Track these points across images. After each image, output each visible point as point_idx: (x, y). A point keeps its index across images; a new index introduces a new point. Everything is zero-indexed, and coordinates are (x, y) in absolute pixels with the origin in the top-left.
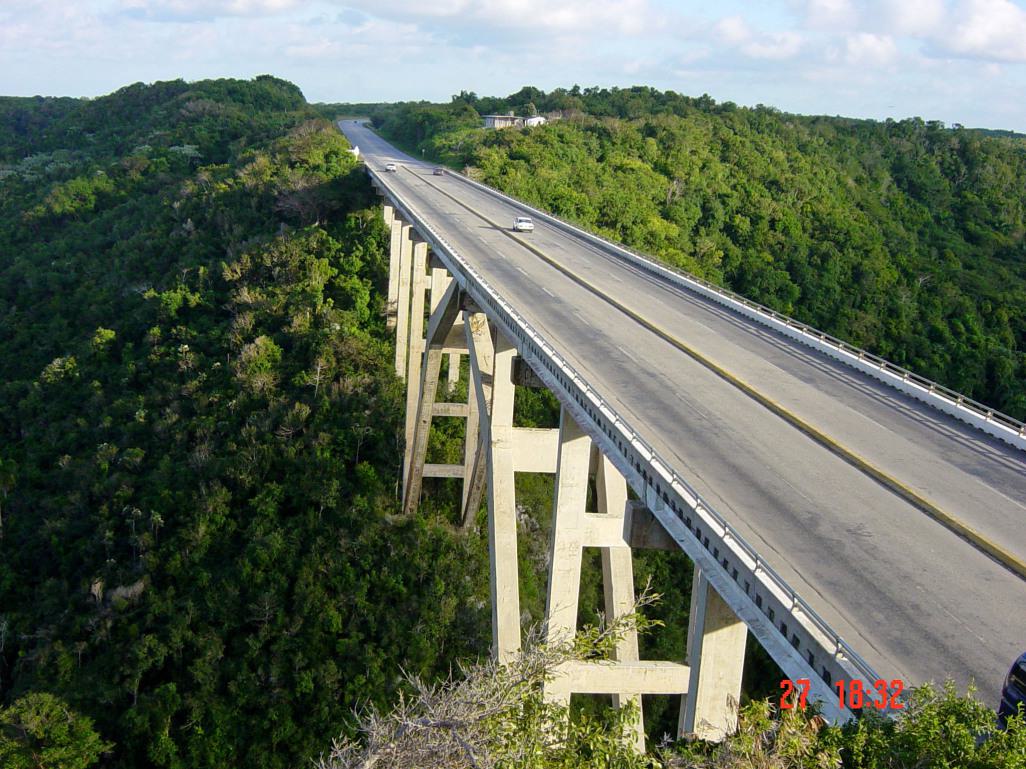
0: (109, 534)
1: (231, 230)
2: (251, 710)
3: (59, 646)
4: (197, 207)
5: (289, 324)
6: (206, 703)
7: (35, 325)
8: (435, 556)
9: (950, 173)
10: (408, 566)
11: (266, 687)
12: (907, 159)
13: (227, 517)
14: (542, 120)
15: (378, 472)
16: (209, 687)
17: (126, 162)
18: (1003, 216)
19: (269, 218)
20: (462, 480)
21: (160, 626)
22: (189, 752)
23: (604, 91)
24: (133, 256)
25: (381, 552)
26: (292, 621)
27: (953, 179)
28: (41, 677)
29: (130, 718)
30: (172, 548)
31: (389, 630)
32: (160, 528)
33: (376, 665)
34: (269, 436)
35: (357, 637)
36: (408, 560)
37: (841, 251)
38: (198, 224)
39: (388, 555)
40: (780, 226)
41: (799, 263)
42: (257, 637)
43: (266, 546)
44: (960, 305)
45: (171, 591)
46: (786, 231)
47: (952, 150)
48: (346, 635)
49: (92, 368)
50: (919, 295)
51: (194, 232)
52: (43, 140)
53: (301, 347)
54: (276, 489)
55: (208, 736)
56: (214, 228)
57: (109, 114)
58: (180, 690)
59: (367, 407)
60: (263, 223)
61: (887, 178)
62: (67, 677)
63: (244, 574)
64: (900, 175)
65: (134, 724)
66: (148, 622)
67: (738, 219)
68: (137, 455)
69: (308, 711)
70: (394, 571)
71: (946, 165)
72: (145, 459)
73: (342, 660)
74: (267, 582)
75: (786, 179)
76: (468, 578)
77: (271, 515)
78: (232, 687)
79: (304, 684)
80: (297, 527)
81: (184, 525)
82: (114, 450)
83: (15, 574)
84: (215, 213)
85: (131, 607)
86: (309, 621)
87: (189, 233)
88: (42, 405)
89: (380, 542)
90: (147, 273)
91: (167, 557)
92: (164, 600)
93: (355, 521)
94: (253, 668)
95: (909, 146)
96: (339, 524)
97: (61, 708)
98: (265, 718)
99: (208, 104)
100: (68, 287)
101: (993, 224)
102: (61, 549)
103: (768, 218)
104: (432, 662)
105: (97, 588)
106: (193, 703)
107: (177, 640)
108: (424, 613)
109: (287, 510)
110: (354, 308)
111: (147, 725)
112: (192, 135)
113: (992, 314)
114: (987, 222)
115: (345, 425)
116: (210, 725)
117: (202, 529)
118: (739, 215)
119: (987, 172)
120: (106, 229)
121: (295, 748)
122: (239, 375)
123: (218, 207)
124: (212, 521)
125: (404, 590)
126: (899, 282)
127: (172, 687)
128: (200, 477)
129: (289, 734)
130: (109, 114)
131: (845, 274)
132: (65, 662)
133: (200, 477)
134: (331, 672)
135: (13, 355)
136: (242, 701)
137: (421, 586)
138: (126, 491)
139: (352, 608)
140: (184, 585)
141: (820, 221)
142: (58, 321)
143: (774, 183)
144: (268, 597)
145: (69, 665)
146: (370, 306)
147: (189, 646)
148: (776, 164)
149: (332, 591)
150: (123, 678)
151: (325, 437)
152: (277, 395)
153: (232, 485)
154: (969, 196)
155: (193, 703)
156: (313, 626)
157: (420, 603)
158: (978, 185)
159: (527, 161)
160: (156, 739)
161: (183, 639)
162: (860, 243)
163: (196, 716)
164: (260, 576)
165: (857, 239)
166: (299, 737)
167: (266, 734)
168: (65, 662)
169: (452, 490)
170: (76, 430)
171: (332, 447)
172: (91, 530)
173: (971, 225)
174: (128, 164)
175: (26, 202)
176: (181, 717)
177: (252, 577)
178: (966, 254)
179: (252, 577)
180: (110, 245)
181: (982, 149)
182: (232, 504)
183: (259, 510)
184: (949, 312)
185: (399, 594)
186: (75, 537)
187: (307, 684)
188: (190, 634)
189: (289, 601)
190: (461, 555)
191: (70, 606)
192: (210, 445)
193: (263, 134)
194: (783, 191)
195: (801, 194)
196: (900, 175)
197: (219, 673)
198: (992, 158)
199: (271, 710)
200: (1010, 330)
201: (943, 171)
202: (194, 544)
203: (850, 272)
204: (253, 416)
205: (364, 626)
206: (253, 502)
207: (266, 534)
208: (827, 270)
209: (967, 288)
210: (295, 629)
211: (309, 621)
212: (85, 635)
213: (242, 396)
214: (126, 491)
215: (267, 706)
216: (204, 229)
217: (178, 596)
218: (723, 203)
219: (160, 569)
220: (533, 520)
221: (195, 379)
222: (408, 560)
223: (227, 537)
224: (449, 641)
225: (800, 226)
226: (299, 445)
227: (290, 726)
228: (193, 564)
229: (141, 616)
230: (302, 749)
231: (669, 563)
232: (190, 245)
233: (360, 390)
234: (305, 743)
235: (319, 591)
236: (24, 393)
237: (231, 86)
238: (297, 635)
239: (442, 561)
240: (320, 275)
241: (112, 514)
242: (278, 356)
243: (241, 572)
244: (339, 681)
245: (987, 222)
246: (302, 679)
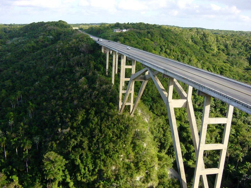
1: (70, 55)
5: (88, 74)
8: (129, 121)
10: (124, 123)
12: (193, 36)
14: (126, 30)
18: (212, 47)
20: (130, 106)
21: (75, 137)
23: (134, 23)
27: (202, 40)
31: (122, 136)
34: (90, 98)
37: (187, 56)
38: (62, 53)
41: (179, 59)
47: (202, 34)
50: (201, 64)
51: (61, 56)
54: (94, 109)
56: (66, 55)
57: (29, 29)
58: (81, 150)
59: (109, 91)
62: (55, 148)
64: (193, 40)
67: (167, 50)
73: (114, 142)
75: (175, 42)
76: (135, 125)
78: (92, 149)
82: (55, 101)
87: (60, 56)
88: (34, 92)
89: (118, 119)
91: (73, 123)
95: (194, 34)
96: (108, 115)
97: (56, 155)
99: (52, 27)
100: (35, 67)
102: (47, 122)
103: (173, 50)
105: (60, 130)
108: (129, 132)
110: (100, 71)
111: (74, 157)
114: (209, 49)
115: (106, 95)
116: (87, 156)
117: (80, 117)
118: (167, 49)
122: (80, 85)
123: (66, 50)
124: (81, 116)
126: (198, 62)
128: (76, 107)
131: (188, 60)
133: (76, 107)
134: (112, 145)
135: (25, 81)
136: (94, 151)
137: (127, 127)
138: (61, 110)
139: (113, 132)
141: (182, 50)
143: (173, 42)
144: (97, 131)
145: (55, 146)
146: (103, 70)
147: (81, 141)
148: (173, 39)
151: (102, 98)
154: (206, 43)
155: (83, 152)
158: (207, 42)
159: (128, 40)
160: (76, 160)
163: (84, 155)
166: (106, 158)
167: (100, 158)
168: (55, 145)
172: (54, 118)
173: (207, 49)
174: (38, 40)
175: (17, 48)
176: (81, 155)
179: (92, 127)
181: (208, 34)
184: (207, 67)
189: (100, 131)
193: (67, 34)
196: (193, 40)
198: (210, 36)
201: (200, 39)
202: (79, 120)
203: (189, 60)
204: (85, 94)
206: (89, 111)
207: (93, 117)
208: (184, 60)
210: (103, 137)
211: (106, 135)
212: (58, 140)
218: (164, 47)
219: (72, 125)
220: (142, 113)
221: (70, 86)
225: (178, 51)
226: (97, 100)
227: (104, 156)
228: (79, 124)
231: (165, 119)
232: (61, 58)
234: (107, 159)
240: (92, 63)
241: (59, 115)
245: (209, 49)
246: (106, 146)
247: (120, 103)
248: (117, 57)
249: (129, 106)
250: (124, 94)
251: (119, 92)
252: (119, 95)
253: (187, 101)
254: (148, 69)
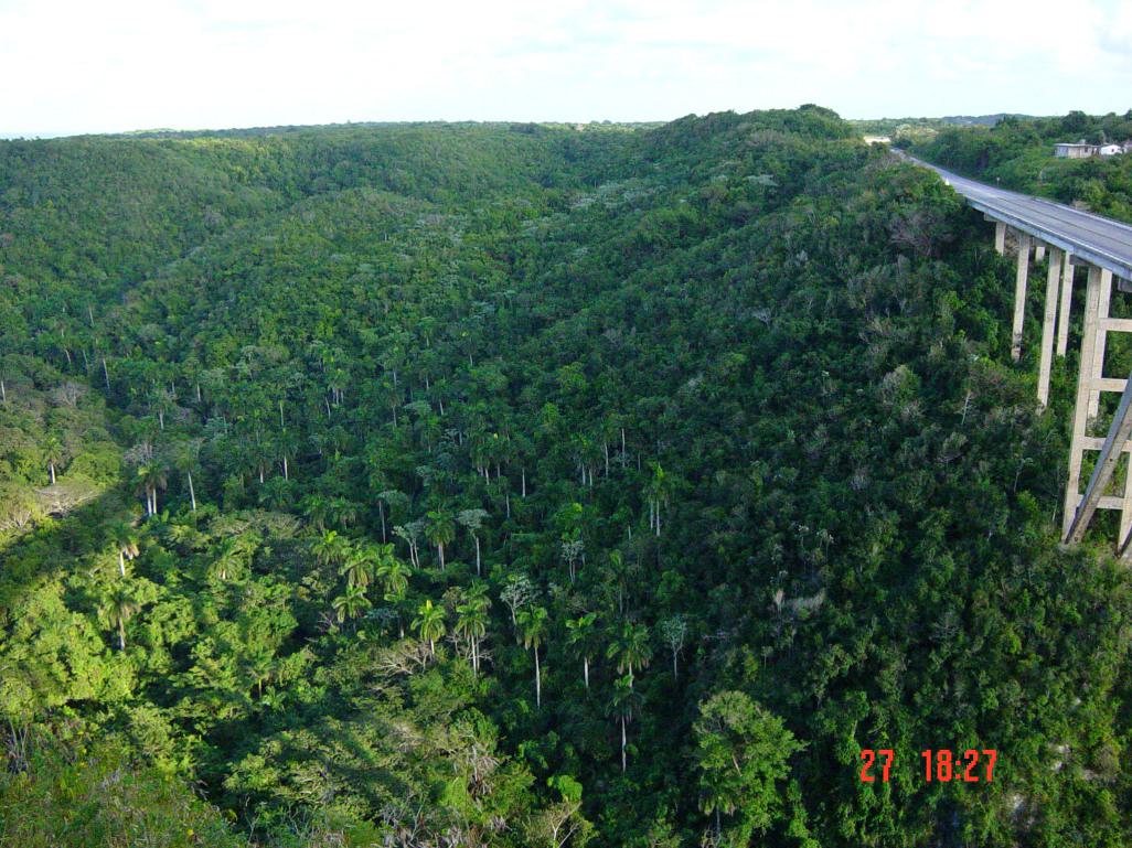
0: (777, 547)
1: (846, 261)
2: (935, 721)
3: (745, 649)
4: (808, 238)
5: (924, 353)
8: (1109, 585)
10: (1083, 594)
11: (949, 701)
13: (895, 537)
15: (1038, 500)
17: (706, 192)
21: (845, 637)
24: (750, 283)
25: (1056, 579)
26: (973, 640)
28: (726, 675)
32: (831, 545)
33: (1059, 687)
38: (811, 254)
43: (940, 567)
45: (849, 605)
49: (726, 389)
52: (608, 169)
53: (940, 376)
56: (827, 258)
57: (667, 143)
58: (870, 699)
60: (876, 255)
62: (753, 678)
69: (993, 725)
70: (1069, 598)
72: (799, 479)
73: (1025, 680)
78: (918, 698)
79: (989, 701)
80: (964, 551)
81: (855, 544)
82: (766, 467)
84: (828, 245)
85: (813, 617)
86: (990, 642)
87: (803, 263)
89: (1054, 570)
91: (841, 573)
92: (844, 613)
93: (1024, 548)
94: (937, 681)
97: (755, 707)
98: (950, 729)
99: (771, 134)
100: (686, 312)
104: (1109, 687)
105: (778, 597)
111: (834, 727)
112: (765, 166)
116: (895, 731)
117: (876, 549)
120: (715, 257)
125: (1079, 616)
130: (667, 143)
132: (752, 665)
134: (1015, 692)
136: (926, 712)
137: (1096, 614)
139: (1029, 632)
144: (950, 617)
145: (755, 667)
146: (998, 337)
149: (1010, 615)
150: (811, 681)
151: (984, 465)
153: (903, 509)
156: (993, 646)
157: (1099, 631)
160: (844, 742)
161: (868, 651)
163: (881, 723)
164: (936, 596)
168: (752, 665)
169: (1106, 519)
172: (758, 543)
179: (929, 597)
180: (721, 273)
182: (900, 526)
185: (1074, 621)
187: (991, 701)
189: (967, 619)
205: (1042, 649)
206: (921, 525)
210: (976, 649)
211: (990, 642)
212: (771, 641)
213: (892, 424)
214: (789, 508)
219: (837, 582)
223: (895, 556)
233: (1013, 421)
236: (661, 409)
237: (785, 117)
238: (978, 654)
241: (778, 529)
242: (918, 383)
247: (1073, 498)
248: (1069, 275)
252: (1065, 457)
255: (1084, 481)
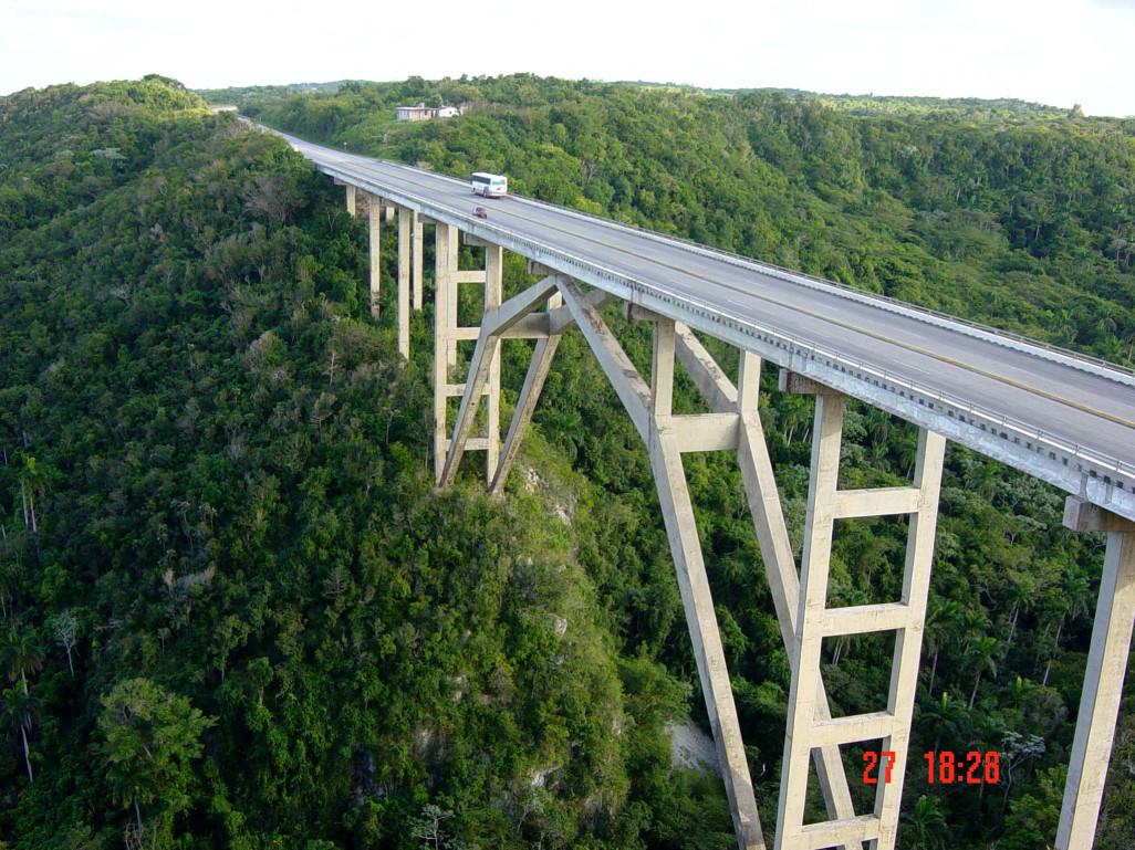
6: (295, 672)
7: (13, 333)
8: (484, 523)
9: (795, 138)
11: (349, 653)
12: (759, 129)
13: (277, 502)
16: (297, 658)
18: (844, 175)
19: (237, 218)
20: (485, 452)
22: (285, 717)
23: (490, 78)
24: (106, 261)
25: (435, 522)
26: (364, 590)
27: (800, 144)
29: (226, 693)
30: (232, 535)
31: (455, 591)
35: (426, 600)
36: (459, 528)
38: (165, 227)
39: (441, 524)
40: (678, 197)
42: (333, 609)
44: (835, 259)
45: (240, 574)
46: (684, 201)
48: (414, 599)
51: (163, 236)
55: (301, 701)
56: (183, 231)
58: (272, 664)
60: (231, 223)
61: (747, 146)
63: (309, 553)
65: (230, 698)
66: (227, 605)
67: (644, 193)
68: (164, 451)
69: (394, 669)
71: (792, 131)
73: (417, 622)
74: (333, 558)
76: (514, 538)
77: (321, 498)
79: (387, 646)
83: (66, 571)
85: (206, 592)
86: (380, 590)
87: (158, 236)
88: (45, 409)
89: (431, 514)
90: (122, 277)
91: (228, 543)
94: (335, 636)
95: (759, 116)
96: (388, 499)
100: (40, 296)
101: (839, 183)
103: (668, 191)
106: (283, 673)
107: (258, 618)
109: (333, 491)
113: (860, 265)
116: (302, 691)
117: (260, 515)
119: (828, 137)
121: (385, 703)
123: (183, 210)
125: (459, 553)
126: (782, 242)
127: (265, 660)
129: (378, 692)
136: (329, 667)
137: (474, 550)
138: (168, 485)
140: (253, 568)
142: (36, 329)
144: (339, 572)
145: (153, 651)
147: (269, 623)
149: (396, 561)
150: (211, 656)
152: (296, 387)
154: (815, 158)
157: (479, 565)
160: (253, 710)
162: (747, 209)
163: (287, 684)
164: (324, 555)
165: (744, 206)
166: (387, 692)
170: (91, 430)
171: (364, 430)
172: (141, 524)
176: (276, 685)
177: (316, 554)
178: (826, 212)
179: (316, 554)
180: (73, 251)
182: (281, 490)
183: (309, 493)
185: (456, 559)
186: (123, 533)
187: (388, 646)
188: (269, 612)
190: (506, 520)
191: (140, 596)
192: (245, 438)
194: (676, 166)
195: (692, 167)
197: (303, 644)
199: (359, 672)
200: (876, 278)
201: (790, 138)
204: (279, 408)
205: (430, 590)
206: (302, 486)
208: (723, 235)
209: (837, 242)
210: (369, 599)
211: (380, 590)
213: (262, 390)
215: (354, 669)
216: (172, 232)
217: (248, 578)
218: (630, 180)
220: (543, 480)
222: (459, 528)
224: (506, 595)
226: (333, 430)
229: (217, 599)
230: (392, 702)
231: (648, 507)
232: (161, 248)
235: (385, 563)
236: (23, 399)
238: (371, 603)
239: (491, 525)
243: (306, 551)
244: (418, 640)
247: (442, 443)
249: (482, 456)
250: (454, 402)
251: (431, 392)
252: (431, 406)
253: (740, 419)
254: (559, 284)
255: (450, 425)
